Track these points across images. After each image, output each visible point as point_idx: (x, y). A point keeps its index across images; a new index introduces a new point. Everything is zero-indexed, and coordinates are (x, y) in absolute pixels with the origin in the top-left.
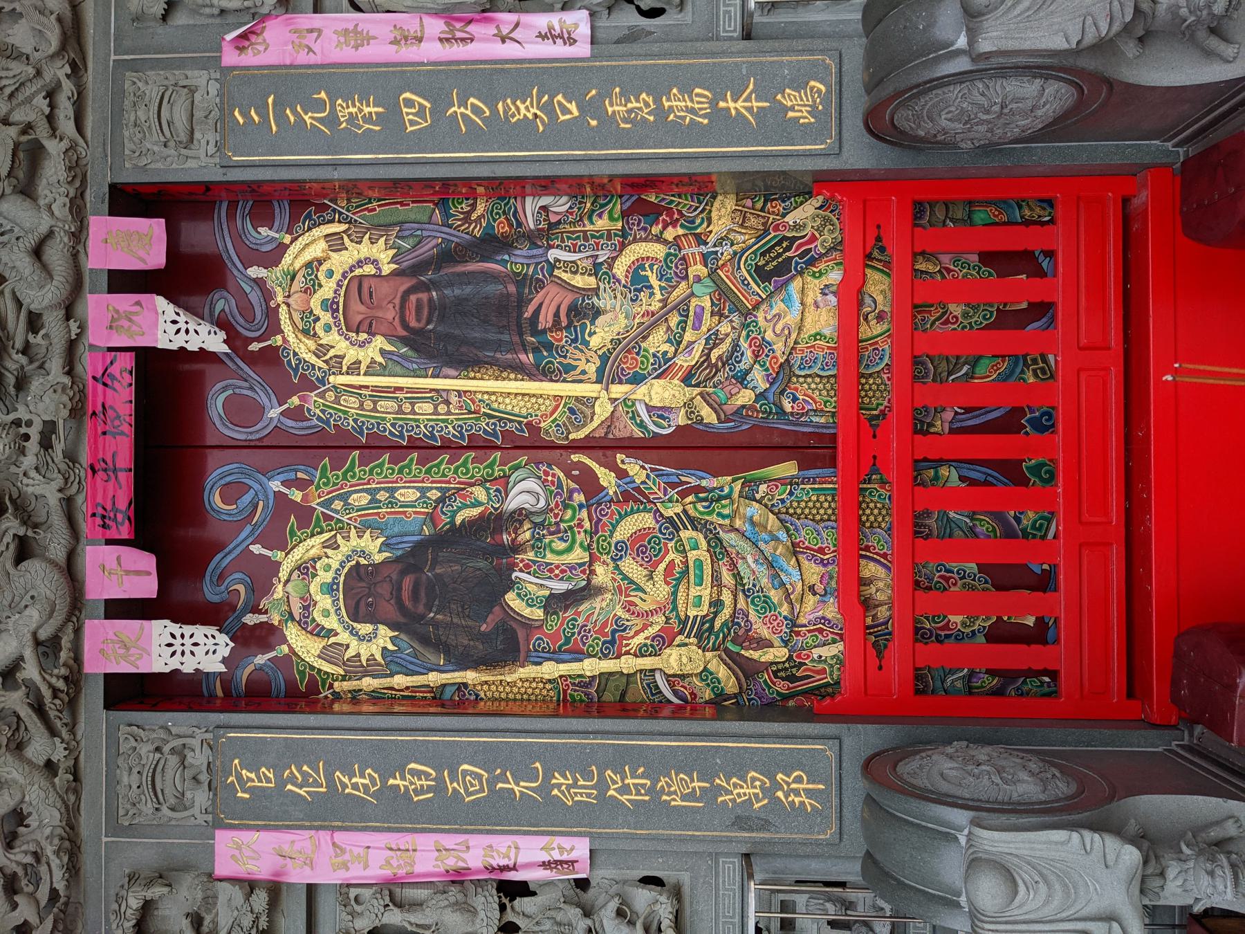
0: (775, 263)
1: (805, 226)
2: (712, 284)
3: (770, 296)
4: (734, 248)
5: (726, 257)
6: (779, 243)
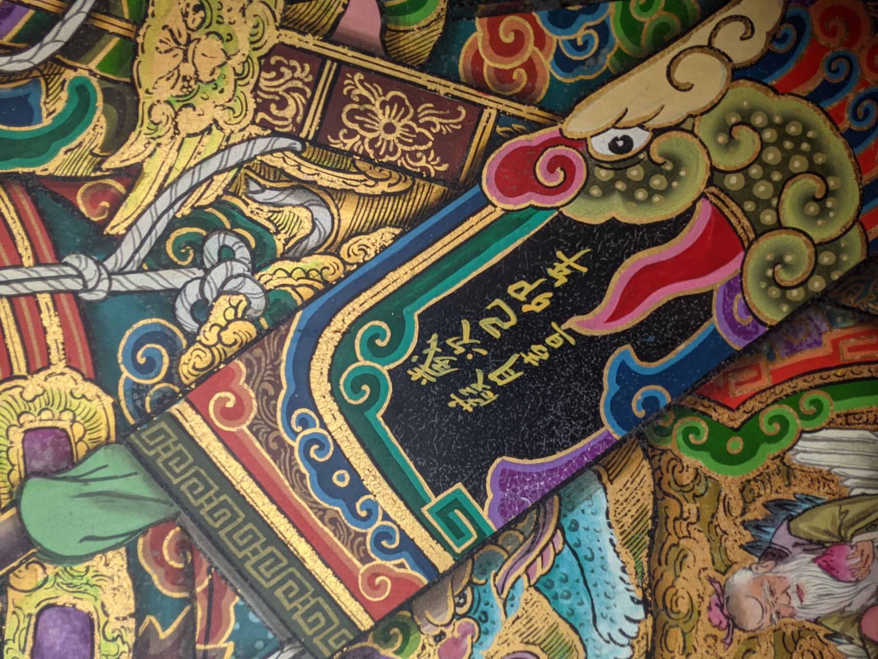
0: (505, 374)
1: (673, 169)
2: (138, 485)
3: (478, 557)
4: (275, 276)
5: (226, 326)
6: (531, 261)
